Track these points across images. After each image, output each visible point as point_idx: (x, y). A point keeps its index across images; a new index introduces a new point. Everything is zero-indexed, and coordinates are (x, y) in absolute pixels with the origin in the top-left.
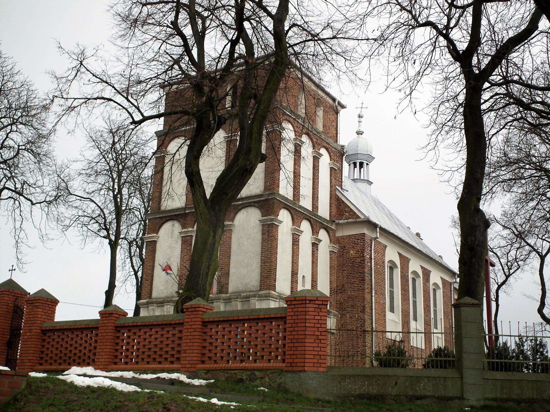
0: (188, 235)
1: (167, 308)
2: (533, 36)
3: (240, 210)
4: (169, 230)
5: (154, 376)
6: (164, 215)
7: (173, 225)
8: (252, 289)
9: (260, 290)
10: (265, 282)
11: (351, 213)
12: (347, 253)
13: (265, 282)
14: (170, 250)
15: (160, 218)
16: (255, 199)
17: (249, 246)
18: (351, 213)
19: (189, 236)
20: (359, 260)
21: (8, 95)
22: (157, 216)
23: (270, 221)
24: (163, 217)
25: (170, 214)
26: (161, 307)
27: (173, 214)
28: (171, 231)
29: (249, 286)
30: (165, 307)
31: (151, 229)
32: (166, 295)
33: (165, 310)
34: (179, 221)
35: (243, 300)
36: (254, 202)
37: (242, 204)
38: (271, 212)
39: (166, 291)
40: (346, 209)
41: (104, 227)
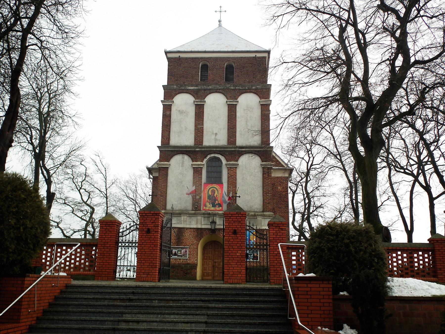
0: (199, 167)
1: (184, 219)
2: (253, 55)
3: (243, 154)
4: (179, 161)
5: (307, 275)
6: (176, 149)
7: (183, 158)
8: (256, 210)
9: (263, 211)
10: (268, 207)
11: (277, 163)
12: (276, 188)
13: (268, 207)
14: (181, 175)
15: (172, 151)
16: (256, 149)
17: (251, 181)
18: (277, 163)
19: (200, 167)
20: (284, 193)
21: (412, 83)
22: (169, 149)
23: (270, 166)
24: (175, 150)
25: (182, 150)
26: (176, 217)
27: (184, 150)
28: (181, 162)
29: (253, 208)
30: (182, 217)
31: (163, 158)
32: (180, 208)
33: (182, 219)
34: (190, 156)
35: (250, 217)
36: (255, 151)
37: (245, 151)
38: (270, 160)
39: (179, 206)
40: (274, 160)
41: (30, 142)
